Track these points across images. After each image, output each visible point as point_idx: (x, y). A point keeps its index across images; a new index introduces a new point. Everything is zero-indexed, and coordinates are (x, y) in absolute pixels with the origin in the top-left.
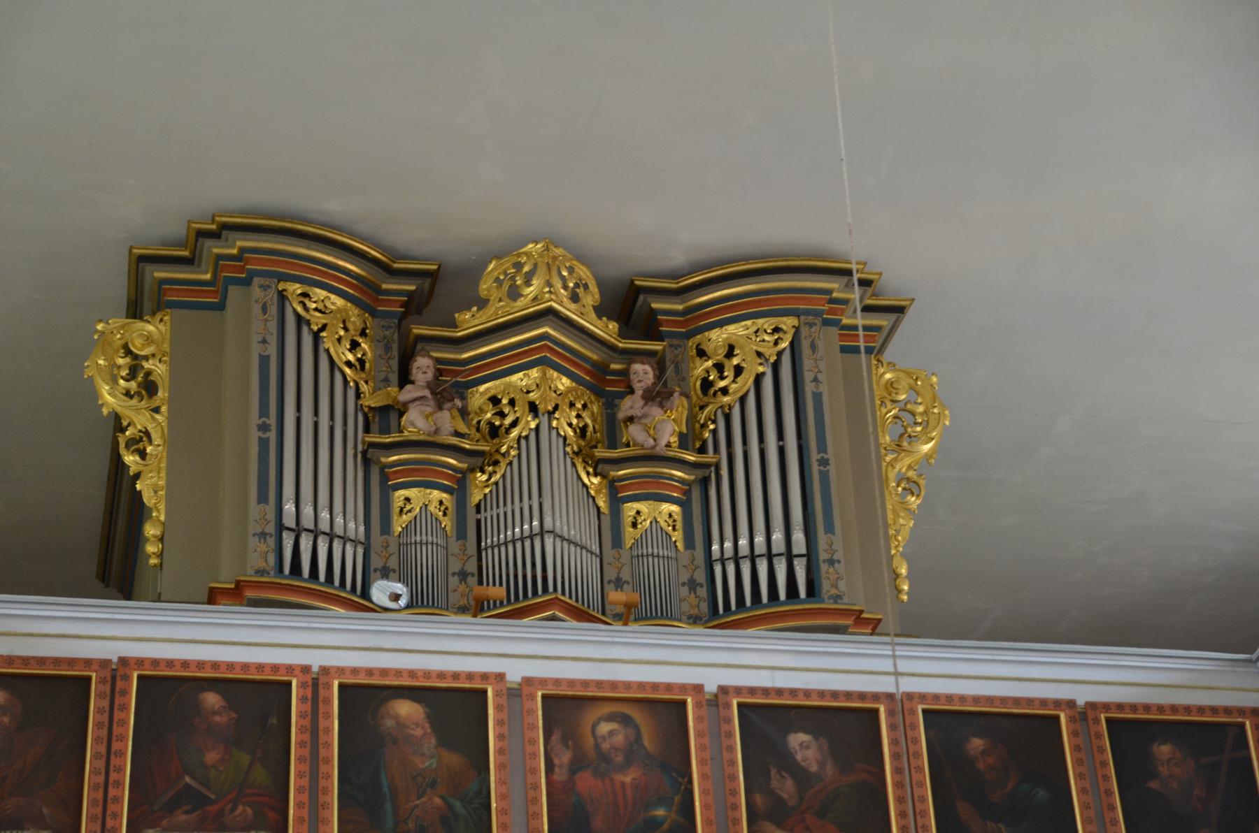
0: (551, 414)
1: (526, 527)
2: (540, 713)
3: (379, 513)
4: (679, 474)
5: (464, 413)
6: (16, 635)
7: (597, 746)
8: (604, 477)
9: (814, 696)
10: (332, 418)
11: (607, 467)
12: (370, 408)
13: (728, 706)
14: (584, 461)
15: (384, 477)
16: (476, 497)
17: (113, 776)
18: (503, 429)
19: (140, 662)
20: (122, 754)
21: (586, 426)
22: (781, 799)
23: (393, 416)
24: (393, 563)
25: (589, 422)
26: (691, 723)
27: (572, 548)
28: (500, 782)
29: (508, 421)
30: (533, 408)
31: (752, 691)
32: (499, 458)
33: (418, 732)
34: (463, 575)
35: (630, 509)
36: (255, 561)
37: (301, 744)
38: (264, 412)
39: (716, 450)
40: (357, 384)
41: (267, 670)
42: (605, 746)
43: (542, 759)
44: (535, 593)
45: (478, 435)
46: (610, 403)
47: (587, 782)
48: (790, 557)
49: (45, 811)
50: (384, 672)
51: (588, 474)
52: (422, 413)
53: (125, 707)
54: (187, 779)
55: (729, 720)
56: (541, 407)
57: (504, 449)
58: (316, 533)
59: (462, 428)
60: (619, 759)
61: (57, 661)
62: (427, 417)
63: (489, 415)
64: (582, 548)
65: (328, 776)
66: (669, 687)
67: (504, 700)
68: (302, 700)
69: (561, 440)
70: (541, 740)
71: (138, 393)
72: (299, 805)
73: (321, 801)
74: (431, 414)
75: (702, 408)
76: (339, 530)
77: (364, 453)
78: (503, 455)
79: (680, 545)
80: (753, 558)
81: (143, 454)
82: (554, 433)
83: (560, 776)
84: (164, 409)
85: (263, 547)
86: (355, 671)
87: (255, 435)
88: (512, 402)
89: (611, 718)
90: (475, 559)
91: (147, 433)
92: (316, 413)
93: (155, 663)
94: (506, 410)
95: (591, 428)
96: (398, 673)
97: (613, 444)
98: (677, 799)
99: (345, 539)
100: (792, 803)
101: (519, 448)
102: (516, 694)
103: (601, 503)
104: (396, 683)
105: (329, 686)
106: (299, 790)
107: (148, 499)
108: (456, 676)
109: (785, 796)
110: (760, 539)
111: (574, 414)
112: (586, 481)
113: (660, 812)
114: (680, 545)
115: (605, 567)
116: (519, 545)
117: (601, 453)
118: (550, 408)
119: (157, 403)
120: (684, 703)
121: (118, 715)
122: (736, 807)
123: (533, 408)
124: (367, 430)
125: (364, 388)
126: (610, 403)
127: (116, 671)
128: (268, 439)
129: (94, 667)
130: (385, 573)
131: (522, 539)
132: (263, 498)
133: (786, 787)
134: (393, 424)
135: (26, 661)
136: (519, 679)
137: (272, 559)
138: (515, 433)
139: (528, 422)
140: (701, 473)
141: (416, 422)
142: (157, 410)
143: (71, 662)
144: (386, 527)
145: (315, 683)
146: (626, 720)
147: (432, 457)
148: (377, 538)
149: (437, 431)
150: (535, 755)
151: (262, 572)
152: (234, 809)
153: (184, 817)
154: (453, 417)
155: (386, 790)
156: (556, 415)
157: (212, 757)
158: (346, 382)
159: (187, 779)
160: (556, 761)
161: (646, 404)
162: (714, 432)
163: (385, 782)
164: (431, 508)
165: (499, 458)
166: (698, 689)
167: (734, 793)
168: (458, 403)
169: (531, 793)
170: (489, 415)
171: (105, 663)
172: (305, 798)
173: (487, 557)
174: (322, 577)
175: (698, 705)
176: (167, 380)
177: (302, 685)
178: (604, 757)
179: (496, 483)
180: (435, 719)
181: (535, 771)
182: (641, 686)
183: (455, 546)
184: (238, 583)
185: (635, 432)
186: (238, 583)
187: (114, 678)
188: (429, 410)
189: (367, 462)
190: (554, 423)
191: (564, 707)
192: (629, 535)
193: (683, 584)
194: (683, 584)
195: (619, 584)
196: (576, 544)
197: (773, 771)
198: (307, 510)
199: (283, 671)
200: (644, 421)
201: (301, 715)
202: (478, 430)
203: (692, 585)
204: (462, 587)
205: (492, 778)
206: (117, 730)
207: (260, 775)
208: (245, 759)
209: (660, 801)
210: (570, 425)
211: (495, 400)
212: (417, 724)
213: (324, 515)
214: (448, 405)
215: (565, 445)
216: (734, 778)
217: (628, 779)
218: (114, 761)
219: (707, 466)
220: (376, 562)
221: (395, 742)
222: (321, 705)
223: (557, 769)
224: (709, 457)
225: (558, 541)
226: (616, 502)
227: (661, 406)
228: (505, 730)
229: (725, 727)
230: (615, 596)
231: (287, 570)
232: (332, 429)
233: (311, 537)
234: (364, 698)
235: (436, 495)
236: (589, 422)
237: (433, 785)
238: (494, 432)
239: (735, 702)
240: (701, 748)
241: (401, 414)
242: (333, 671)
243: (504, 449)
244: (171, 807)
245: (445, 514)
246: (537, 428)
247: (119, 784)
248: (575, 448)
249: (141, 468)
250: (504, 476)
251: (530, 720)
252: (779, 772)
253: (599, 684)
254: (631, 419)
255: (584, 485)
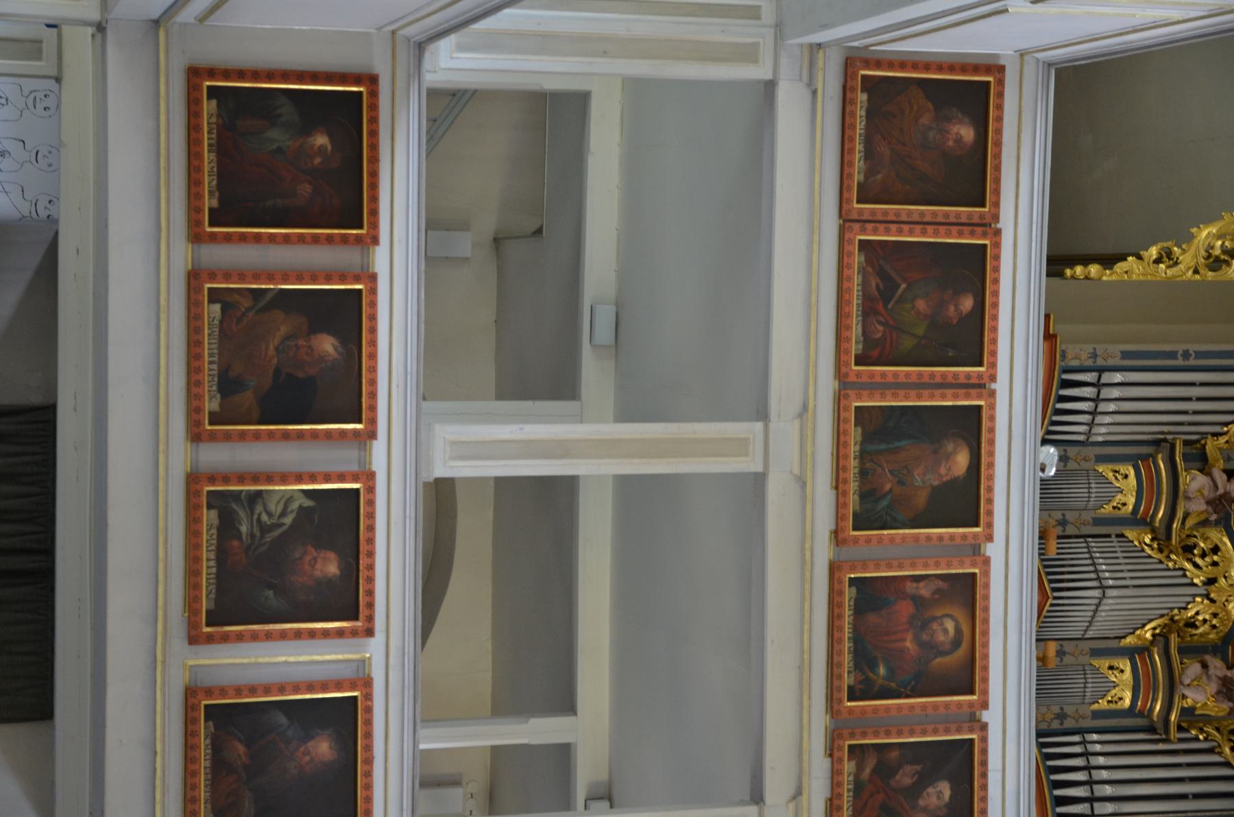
0: (1207, 596)
1: (1107, 574)
2: (961, 571)
3: (1114, 452)
4: (1158, 707)
5: (1204, 523)
6: (1019, 148)
7: (935, 619)
8: (1152, 643)
9: (982, 805)
10: (1196, 413)
11: (1161, 645)
12: (1204, 446)
13: (971, 731)
14: (1165, 625)
15: (1145, 458)
16: (1130, 534)
17: (906, 227)
18: (1190, 556)
19: (997, 245)
20: (924, 233)
21: (1196, 627)
22: (896, 773)
23: (1198, 464)
24: (1072, 465)
25: (1201, 630)
26: (956, 698)
27: (1090, 614)
28: (904, 537)
29: (1199, 561)
30: (1211, 581)
31: (984, 752)
32: (1166, 553)
33: (943, 471)
34: (1063, 523)
35: (1126, 665)
36: (1072, 350)
37: (932, 375)
38: (1200, 355)
39: (1181, 740)
40: (1226, 433)
41: (992, 347)
42: (935, 626)
43: (923, 573)
44: (1051, 581)
45: (1184, 536)
46: (1218, 649)
47: (905, 609)
48: (1091, 800)
49: (879, 177)
50: (992, 442)
51: (1154, 629)
52: (1203, 487)
53: (960, 234)
54: (903, 286)
55: (959, 731)
56: (1213, 588)
57: (1173, 557)
58: (1096, 400)
59: (1190, 522)
60: (925, 637)
61: (997, 181)
62: (1199, 491)
63: (1202, 545)
64: (1090, 622)
65: (907, 398)
66: (985, 680)
67: (970, 541)
68: (968, 376)
69: (1183, 605)
70: (939, 572)
71: (1210, 256)
72: (883, 374)
73: (887, 392)
74: (1203, 495)
75: (1218, 729)
76: (1099, 419)
77: (1165, 440)
78: (1168, 557)
79: (1095, 707)
80: (1088, 768)
81: (1158, 261)
82: (1190, 599)
83: (910, 587)
84: (1197, 277)
85: (1084, 356)
86: (992, 418)
87: (1180, 348)
88: (1215, 564)
89: (958, 630)
90: (1077, 532)
91: (1176, 263)
92: (1199, 399)
93: (997, 258)
94: (1207, 559)
95: (1194, 632)
96: (991, 454)
97: (1182, 651)
98: (893, 685)
99: (1091, 424)
100: (892, 783)
101: (1175, 569)
102: (975, 550)
103: (1129, 640)
104: (983, 451)
105: (979, 397)
106: (896, 374)
107: (1120, 267)
108: (990, 501)
109: (898, 777)
110: (1104, 774)
111: (1207, 617)
112: (1148, 627)
113: (882, 671)
114: (1095, 707)
115: (1075, 642)
116: (1091, 568)
117: (1174, 640)
118: (1212, 595)
119: (1202, 271)
120: (972, 693)
121: (955, 229)
122: (888, 734)
123: (1211, 581)
124: (1186, 443)
125: (1222, 440)
126: (1218, 649)
127: (989, 225)
128: (1176, 358)
129: (993, 210)
130: (1063, 459)
131: (1096, 571)
132: (1126, 355)
133: (905, 778)
134: (1192, 464)
135: (998, 156)
136: (988, 554)
137: (1075, 363)
138: (1188, 566)
139: (1198, 577)
140: (1160, 726)
141: (1194, 482)
142: (1196, 272)
143: (997, 192)
144: (1102, 459)
145: (982, 386)
146: (957, 643)
147: (1164, 497)
148: (1092, 452)
149: (1188, 498)
150: (926, 566)
151: (1063, 355)
152: (880, 323)
153: (874, 285)
154: (1202, 512)
155: (897, 444)
156: (1206, 601)
157: (921, 305)
158: (1226, 424)
159: (903, 286)
160: (922, 584)
161: (1219, 678)
162: (1196, 739)
163: (902, 443)
164: (1119, 496)
165: (1166, 553)
166: (985, 705)
167: (900, 733)
168: (1214, 517)
169: (895, 563)
170: (1202, 545)
171: (996, 218)
172: (890, 379)
173: (1079, 544)
174: (1059, 406)
175: (971, 704)
176: (1219, 278)
177: (980, 376)
178: (925, 625)
179: (1143, 550)
180: (952, 485)
181: (913, 566)
182: (986, 657)
183: (1087, 516)
184: (1055, 336)
185: (1195, 669)
186: (1055, 336)
187: (984, 225)
188: (1206, 493)
189: (1157, 443)
190: (1198, 599)
191: (966, 591)
192: (1103, 664)
193: (1062, 709)
194: (1062, 709)
195: (1061, 653)
196: (1093, 617)
197: (918, 768)
198: (1116, 393)
199: (992, 359)
200: (1204, 678)
201: (956, 375)
202: (1189, 536)
203: (1062, 716)
204: (1053, 522)
205: (907, 531)
206: (942, 229)
207: (907, 343)
208: (920, 331)
209: (891, 671)
210: (1197, 613)
211: (1216, 550)
212: (949, 470)
213: (1112, 407)
214: (1210, 509)
215: (1180, 609)
216: (912, 733)
217: (908, 644)
218: (918, 228)
219: (1167, 731)
220: (1072, 451)
221: (935, 452)
222: (964, 391)
223: (915, 585)
224: (1174, 734)
225: (1095, 601)
226: (1130, 653)
227: (1219, 692)
228: (946, 542)
229: (953, 727)
230: (1052, 647)
231: (1065, 376)
232: (1185, 413)
233: (1093, 396)
234: (970, 425)
235: (1131, 500)
236: (1201, 630)
237: (901, 483)
238: (1188, 549)
239: (974, 736)
240: (935, 706)
241: (1201, 471)
242: (992, 400)
243: (1173, 557)
244: (882, 274)
245: (1114, 508)
246: (1196, 585)
247: (900, 232)
248: (1176, 618)
249: (1146, 260)
250: (1150, 557)
251: (955, 563)
252: (917, 772)
253: (986, 621)
254: (1205, 666)
255: (1144, 625)
